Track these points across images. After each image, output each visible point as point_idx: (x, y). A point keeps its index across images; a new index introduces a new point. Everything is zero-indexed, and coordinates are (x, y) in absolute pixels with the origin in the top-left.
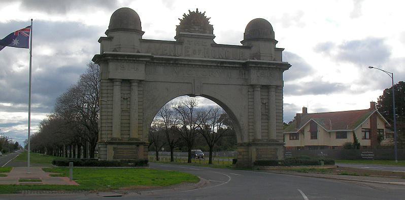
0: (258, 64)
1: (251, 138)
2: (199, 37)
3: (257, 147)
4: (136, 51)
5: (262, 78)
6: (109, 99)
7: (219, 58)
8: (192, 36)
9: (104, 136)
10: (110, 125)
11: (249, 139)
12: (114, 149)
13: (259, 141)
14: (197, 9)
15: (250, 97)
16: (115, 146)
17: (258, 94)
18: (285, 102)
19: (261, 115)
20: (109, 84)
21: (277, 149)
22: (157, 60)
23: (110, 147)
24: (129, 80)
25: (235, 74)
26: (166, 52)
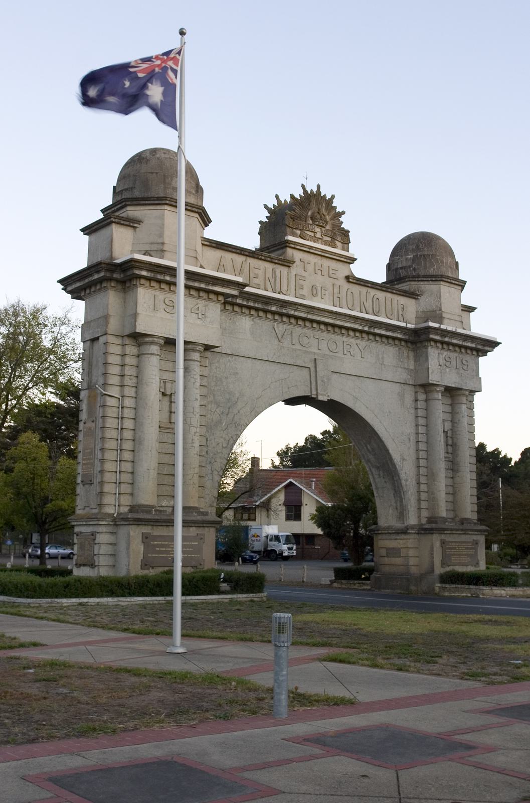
0: (444, 336)
2: (323, 255)
3: (443, 537)
11: (419, 517)
12: (146, 538)
13: (445, 522)
14: (319, 187)
16: (146, 529)
23: (136, 533)
25: (389, 354)
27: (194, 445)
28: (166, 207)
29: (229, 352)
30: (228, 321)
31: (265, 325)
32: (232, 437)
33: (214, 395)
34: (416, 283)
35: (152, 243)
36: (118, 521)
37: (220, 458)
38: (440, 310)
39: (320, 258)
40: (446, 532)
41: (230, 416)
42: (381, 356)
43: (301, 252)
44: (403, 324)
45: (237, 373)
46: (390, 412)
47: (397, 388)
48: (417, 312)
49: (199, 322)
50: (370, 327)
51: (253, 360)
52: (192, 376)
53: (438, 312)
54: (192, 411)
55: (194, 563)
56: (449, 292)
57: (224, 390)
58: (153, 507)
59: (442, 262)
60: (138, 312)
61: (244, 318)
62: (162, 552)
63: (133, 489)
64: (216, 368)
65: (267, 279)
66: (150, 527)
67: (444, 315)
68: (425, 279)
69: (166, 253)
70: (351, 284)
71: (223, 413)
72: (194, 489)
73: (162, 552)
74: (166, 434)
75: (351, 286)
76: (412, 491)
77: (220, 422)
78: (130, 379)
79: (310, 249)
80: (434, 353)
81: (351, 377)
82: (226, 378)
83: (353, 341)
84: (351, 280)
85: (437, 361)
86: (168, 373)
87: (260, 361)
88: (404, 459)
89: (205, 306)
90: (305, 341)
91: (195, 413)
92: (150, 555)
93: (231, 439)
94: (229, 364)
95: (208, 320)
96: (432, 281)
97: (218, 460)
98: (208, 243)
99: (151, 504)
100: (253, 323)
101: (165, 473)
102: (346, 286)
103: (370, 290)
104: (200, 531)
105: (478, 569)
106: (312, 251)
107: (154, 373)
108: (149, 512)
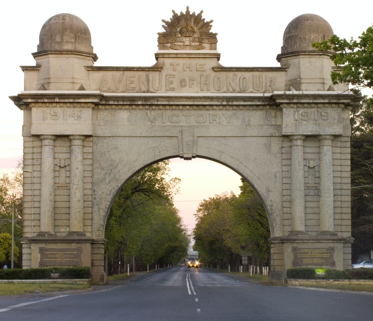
0: (293, 99)
1: (288, 229)
3: (295, 245)
4: (78, 86)
5: (304, 122)
6: (35, 168)
7: (228, 91)
8: (177, 56)
9: (29, 232)
10: (37, 211)
12: (41, 250)
13: (297, 235)
15: (284, 156)
16: (42, 245)
17: (299, 150)
18: (351, 249)
19: (303, 189)
20: (35, 144)
21: (333, 249)
22: (114, 101)
23: (35, 247)
24: (67, 136)
25: (257, 117)
26: (132, 86)
27: (76, 195)
28: (50, 56)
29: (110, 135)
30: (110, 115)
31: (139, 114)
32: (114, 188)
33: (99, 164)
34: (285, 59)
35: (45, 79)
36: (33, 241)
37: (105, 201)
38: (300, 77)
39: (188, 59)
40: (296, 242)
41: (112, 175)
42: (247, 120)
43: (171, 59)
44: (261, 95)
45: (117, 148)
46: (255, 159)
47: (264, 140)
48: (286, 81)
49: (76, 122)
50: (228, 101)
51: (130, 138)
52: (74, 155)
53: (298, 79)
54: (74, 176)
55: (74, 264)
56: (310, 62)
57: (107, 160)
58: (46, 233)
59: (305, 39)
60: (32, 122)
61: (122, 111)
62: (53, 258)
63: (54, 223)
64: (101, 147)
65: (141, 82)
66: (44, 244)
67: (302, 81)
68: (289, 55)
69: (51, 84)
70: (217, 72)
71: (106, 173)
72: (76, 221)
73: (53, 258)
74: (63, 190)
75: (217, 74)
76: (277, 213)
77: (104, 179)
78: (37, 161)
79: (177, 55)
80: (289, 111)
81: (217, 138)
82: (108, 152)
83: (220, 113)
84: (215, 70)
85: (292, 117)
86: (62, 154)
87: (135, 138)
88: (269, 191)
89: (80, 111)
90: (175, 118)
91: (76, 177)
92: (44, 260)
93: (113, 189)
94: (110, 142)
95: (82, 119)
96: (295, 56)
97: (103, 202)
98: (91, 69)
99: (46, 231)
100: (129, 113)
101: (62, 212)
102: (213, 74)
103: (236, 73)
104: (79, 245)
105: (334, 268)
106: (178, 56)
107: (47, 156)
108: (44, 236)
